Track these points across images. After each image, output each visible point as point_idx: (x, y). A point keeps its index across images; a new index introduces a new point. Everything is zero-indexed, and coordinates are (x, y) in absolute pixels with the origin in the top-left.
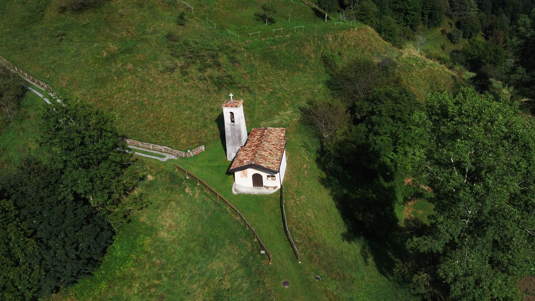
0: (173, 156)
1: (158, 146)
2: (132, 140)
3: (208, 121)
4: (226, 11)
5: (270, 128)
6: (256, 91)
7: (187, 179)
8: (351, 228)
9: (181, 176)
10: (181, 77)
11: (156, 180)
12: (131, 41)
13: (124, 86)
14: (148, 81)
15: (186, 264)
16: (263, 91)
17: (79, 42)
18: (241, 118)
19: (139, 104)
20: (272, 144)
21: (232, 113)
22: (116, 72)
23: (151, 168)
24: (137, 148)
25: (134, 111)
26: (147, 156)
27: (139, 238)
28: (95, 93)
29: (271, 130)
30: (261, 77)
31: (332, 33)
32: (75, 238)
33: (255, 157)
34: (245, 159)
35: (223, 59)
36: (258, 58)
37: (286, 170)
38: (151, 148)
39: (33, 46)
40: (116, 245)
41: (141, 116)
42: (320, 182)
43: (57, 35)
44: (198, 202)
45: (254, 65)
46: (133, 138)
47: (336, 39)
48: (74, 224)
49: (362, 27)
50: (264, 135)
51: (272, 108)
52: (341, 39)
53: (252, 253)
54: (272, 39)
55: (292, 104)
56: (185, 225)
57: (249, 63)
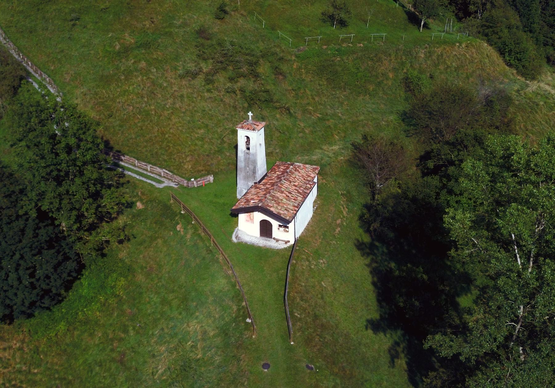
0: (173, 183)
1: (158, 168)
2: (128, 157)
3: (226, 145)
4: (285, 6)
5: (298, 164)
6: (299, 115)
7: (181, 214)
8: (387, 316)
9: (175, 209)
10: (204, 86)
11: (146, 209)
12: (153, 34)
13: (131, 88)
14: (161, 86)
15: (159, 319)
16: (309, 116)
17: (93, 30)
18: (258, 145)
19: (144, 114)
20: (294, 185)
21: (248, 138)
22: (125, 70)
23: (143, 194)
24: (133, 168)
25: (136, 121)
26: (141, 178)
27: (112, 277)
28: (96, 94)
29: (299, 167)
30: (310, 97)
31: (426, 48)
32: (32, 263)
33: (266, 198)
34: (252, 199)
35: (264, 69)
36: (311, 72)
37: (309, 222)
38: (149, 169)
39: (43, 30)
40: (84, 281)
41: (144, 128)
42: (356, 245)
43: (70, 18)
44: (188, 244)
45: (303, 80)
46: (130, 154)
47: (430, 56)
48: (31, 245)
49: (474, 44)
50: (287, 172)
51: (315, 139)
52: (438, 56)
53: (235, 320)
54: (337, 47)
55: (345, 137)
56: (167, 270)
57: (298, 77)
